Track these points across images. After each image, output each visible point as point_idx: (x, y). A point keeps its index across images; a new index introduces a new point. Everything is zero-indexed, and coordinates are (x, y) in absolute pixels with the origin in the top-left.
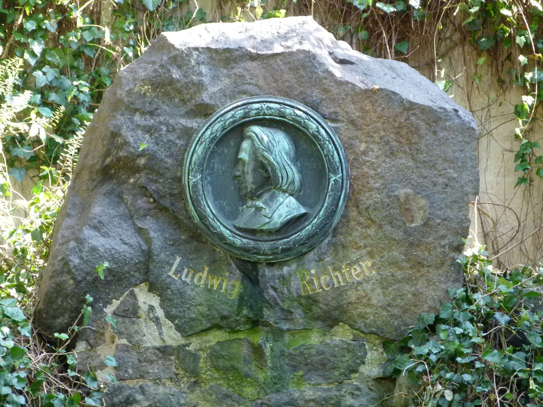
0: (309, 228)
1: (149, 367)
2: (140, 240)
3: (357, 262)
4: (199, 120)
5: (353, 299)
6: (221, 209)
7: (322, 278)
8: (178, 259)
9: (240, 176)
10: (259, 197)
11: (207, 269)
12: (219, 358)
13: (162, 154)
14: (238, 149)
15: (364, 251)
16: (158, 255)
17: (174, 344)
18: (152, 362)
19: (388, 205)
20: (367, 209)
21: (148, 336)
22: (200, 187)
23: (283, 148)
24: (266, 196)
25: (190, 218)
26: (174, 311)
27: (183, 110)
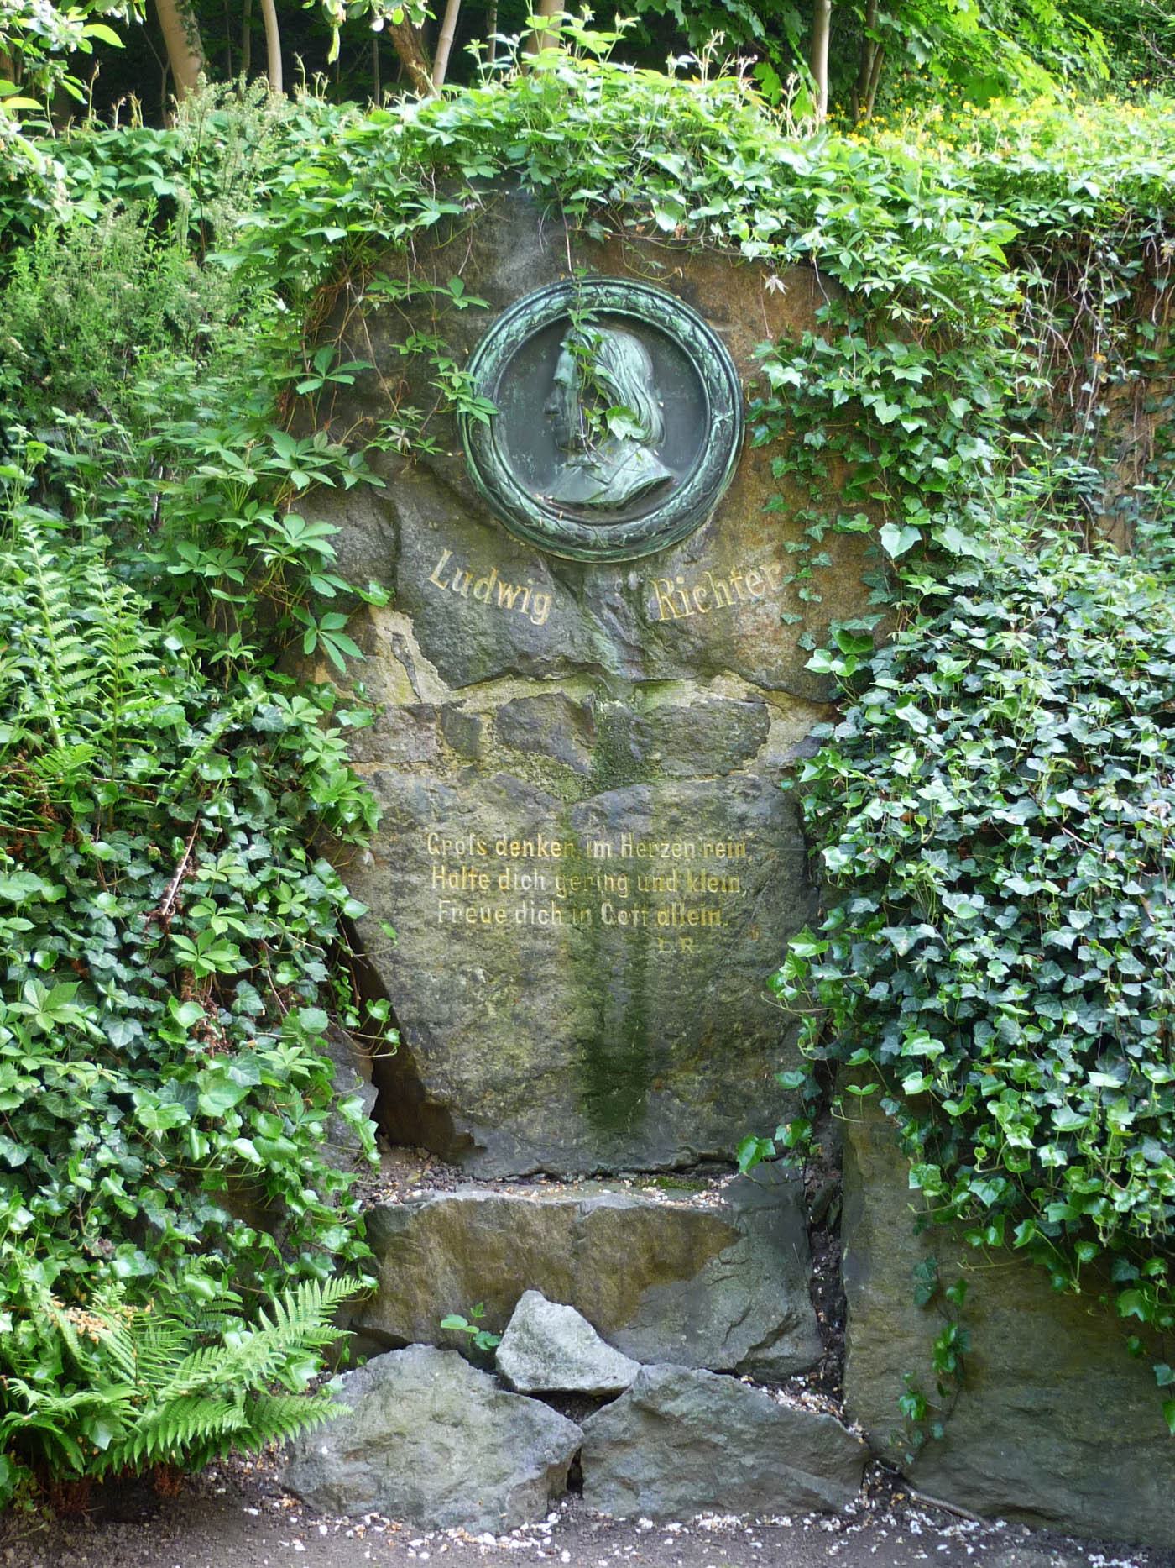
0: (673, 504)
3: (756, 565)
5: (749, 629)
6: (521, 468)
7: (697, 590)
8: (447, 554)
9: (555, 412)
14: (554, 363)
18: (396, 732)
26: (437, 644)
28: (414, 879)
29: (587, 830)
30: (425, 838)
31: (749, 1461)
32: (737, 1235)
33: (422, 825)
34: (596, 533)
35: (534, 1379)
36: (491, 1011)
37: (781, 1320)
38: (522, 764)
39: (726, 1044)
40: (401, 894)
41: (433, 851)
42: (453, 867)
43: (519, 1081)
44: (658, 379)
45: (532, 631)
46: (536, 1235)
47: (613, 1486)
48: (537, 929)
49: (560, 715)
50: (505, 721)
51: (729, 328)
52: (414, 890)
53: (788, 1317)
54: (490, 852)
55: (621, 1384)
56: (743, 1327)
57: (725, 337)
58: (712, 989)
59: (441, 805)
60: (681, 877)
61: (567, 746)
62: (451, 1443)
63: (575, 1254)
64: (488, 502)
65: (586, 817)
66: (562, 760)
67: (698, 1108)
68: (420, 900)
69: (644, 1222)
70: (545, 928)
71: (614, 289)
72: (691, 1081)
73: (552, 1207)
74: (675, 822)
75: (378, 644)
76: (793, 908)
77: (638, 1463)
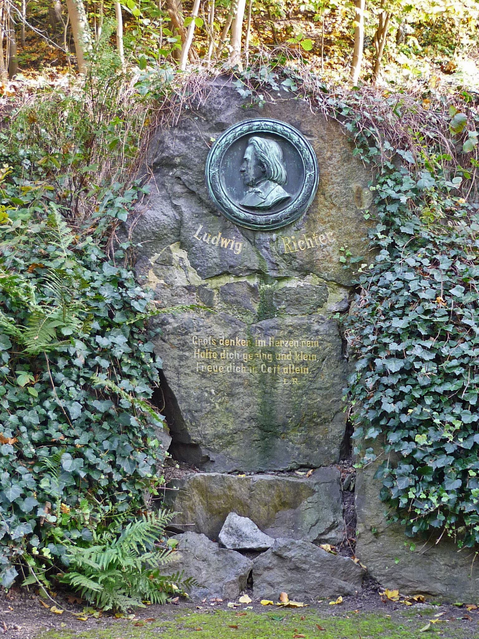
0: (290, 208)
1: (178, 299)
2: (175, 213)
3: (322, 232)
4: (218, 134)
5: (320, 257)
6: (231, 193)
7: (299, 242)
8: (201, 227)
9: (244, 171)
10: (257, 185)
11: (220, 234)
12: (227, 294)
13: (191, 155)
14: (244, 152)
15: (328, 225)
16: (187, 223)
17: (197, 284)
18: (181, 296)
19: (345, 194)
20: (330, 196)
21: (179, 279)
22: (217, 177)
23: (275, 152)
24: (263, 184)
25: (210, 198)
26: (197, 262)
27: (207, 127)
28: (187, 354)
29: (256, 335)
30: (192, 338)
31: (318, 575)
32: (314, 492)
33: (191, 333)
34: (261, 219)
35: (234, 545)
36: (217, 406)
37: (331, 523)
38: (230, 309)
39: (310, 421)
40: (182, 360)
41: (195, 343)
42: (202, 349)
43: (228, 434)
44: (285, 159)
45: (233, 256)
46: (235, 490)
47: (265, 584)
48: (236, 374)
49: (245, 290)
50: (223, 292)
51: (313, 139)
52: (187, 358)
53: (334, 522)
54: (217, 344)
55: (268, 546)
56: (316, 527)
57: (311, 142)
58: (305, 398)
59: (198, 325)
60: (293, 354)
61: (248, 303)
62: (201, 567)
63: (250, 497)
64: (217, 206)
65: (255, 331)
66: (246, 308)
67: (299, 446)
68: (189, 363)
69: (277, 485)
70: (239, 374)
71: (267, 123)
72: (296, 436)
73: (241, 479)
74: (290, 332)
75: (173, 262)
76: (337, 367)
77: (275, 575)
